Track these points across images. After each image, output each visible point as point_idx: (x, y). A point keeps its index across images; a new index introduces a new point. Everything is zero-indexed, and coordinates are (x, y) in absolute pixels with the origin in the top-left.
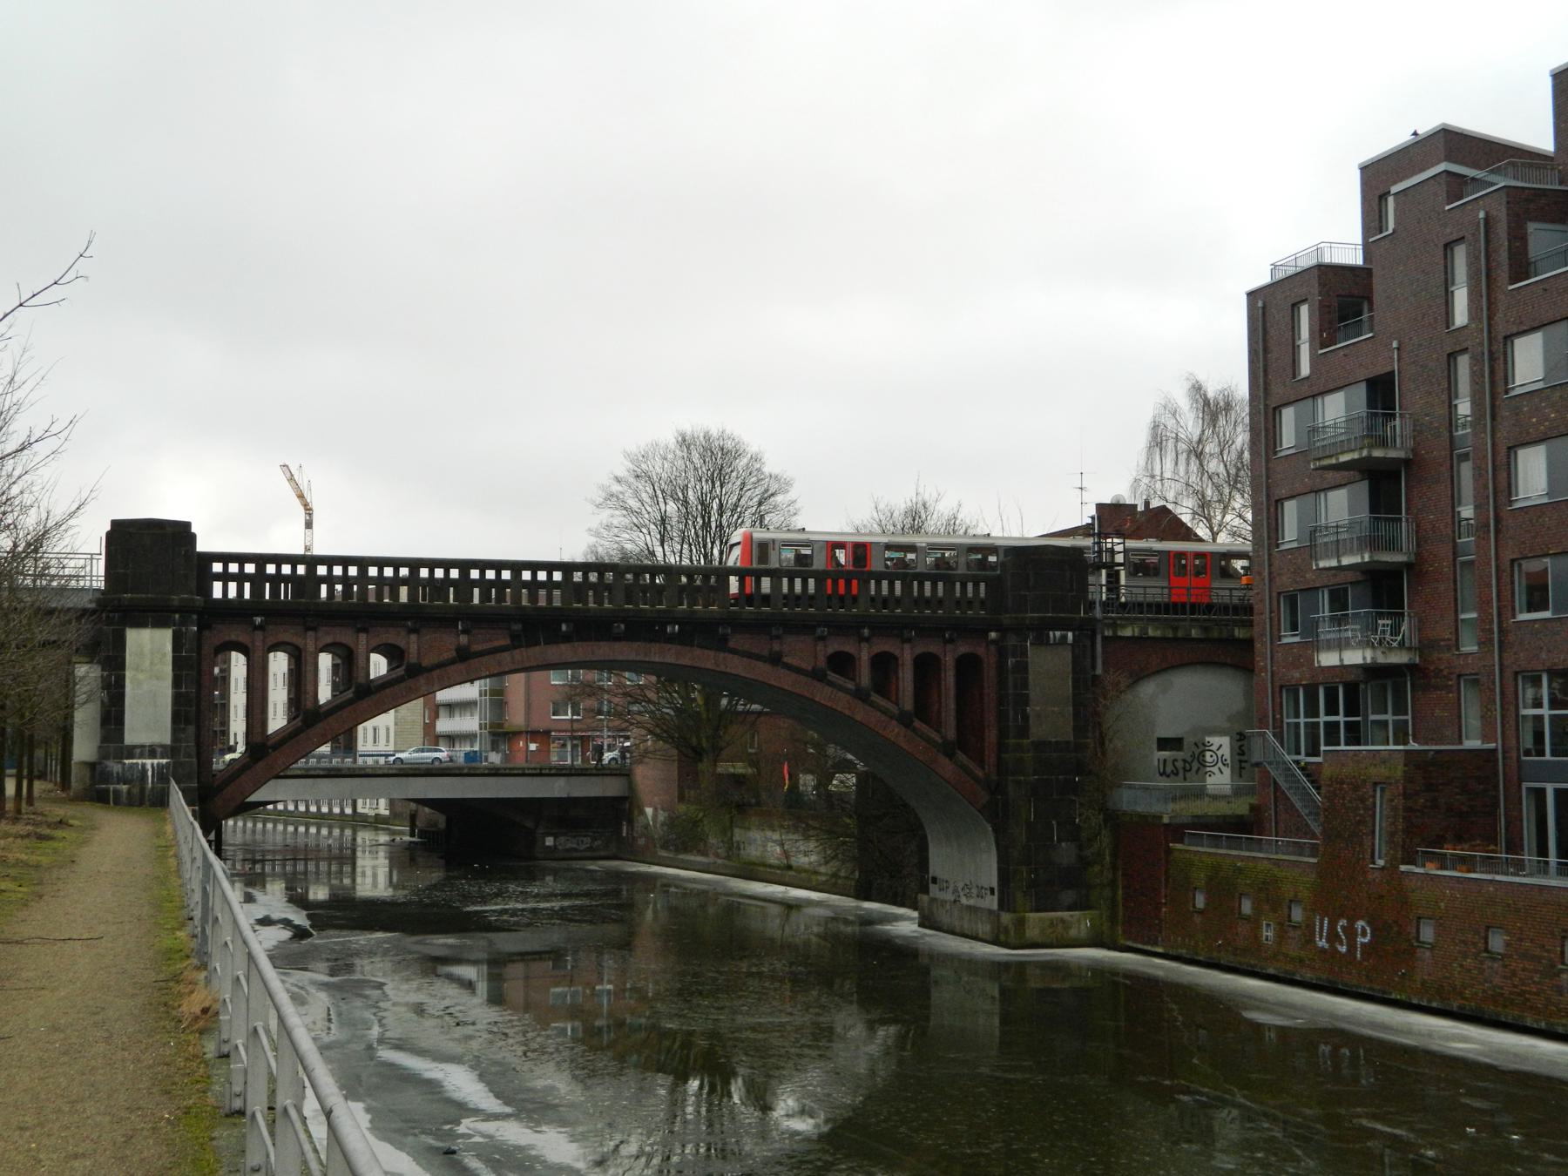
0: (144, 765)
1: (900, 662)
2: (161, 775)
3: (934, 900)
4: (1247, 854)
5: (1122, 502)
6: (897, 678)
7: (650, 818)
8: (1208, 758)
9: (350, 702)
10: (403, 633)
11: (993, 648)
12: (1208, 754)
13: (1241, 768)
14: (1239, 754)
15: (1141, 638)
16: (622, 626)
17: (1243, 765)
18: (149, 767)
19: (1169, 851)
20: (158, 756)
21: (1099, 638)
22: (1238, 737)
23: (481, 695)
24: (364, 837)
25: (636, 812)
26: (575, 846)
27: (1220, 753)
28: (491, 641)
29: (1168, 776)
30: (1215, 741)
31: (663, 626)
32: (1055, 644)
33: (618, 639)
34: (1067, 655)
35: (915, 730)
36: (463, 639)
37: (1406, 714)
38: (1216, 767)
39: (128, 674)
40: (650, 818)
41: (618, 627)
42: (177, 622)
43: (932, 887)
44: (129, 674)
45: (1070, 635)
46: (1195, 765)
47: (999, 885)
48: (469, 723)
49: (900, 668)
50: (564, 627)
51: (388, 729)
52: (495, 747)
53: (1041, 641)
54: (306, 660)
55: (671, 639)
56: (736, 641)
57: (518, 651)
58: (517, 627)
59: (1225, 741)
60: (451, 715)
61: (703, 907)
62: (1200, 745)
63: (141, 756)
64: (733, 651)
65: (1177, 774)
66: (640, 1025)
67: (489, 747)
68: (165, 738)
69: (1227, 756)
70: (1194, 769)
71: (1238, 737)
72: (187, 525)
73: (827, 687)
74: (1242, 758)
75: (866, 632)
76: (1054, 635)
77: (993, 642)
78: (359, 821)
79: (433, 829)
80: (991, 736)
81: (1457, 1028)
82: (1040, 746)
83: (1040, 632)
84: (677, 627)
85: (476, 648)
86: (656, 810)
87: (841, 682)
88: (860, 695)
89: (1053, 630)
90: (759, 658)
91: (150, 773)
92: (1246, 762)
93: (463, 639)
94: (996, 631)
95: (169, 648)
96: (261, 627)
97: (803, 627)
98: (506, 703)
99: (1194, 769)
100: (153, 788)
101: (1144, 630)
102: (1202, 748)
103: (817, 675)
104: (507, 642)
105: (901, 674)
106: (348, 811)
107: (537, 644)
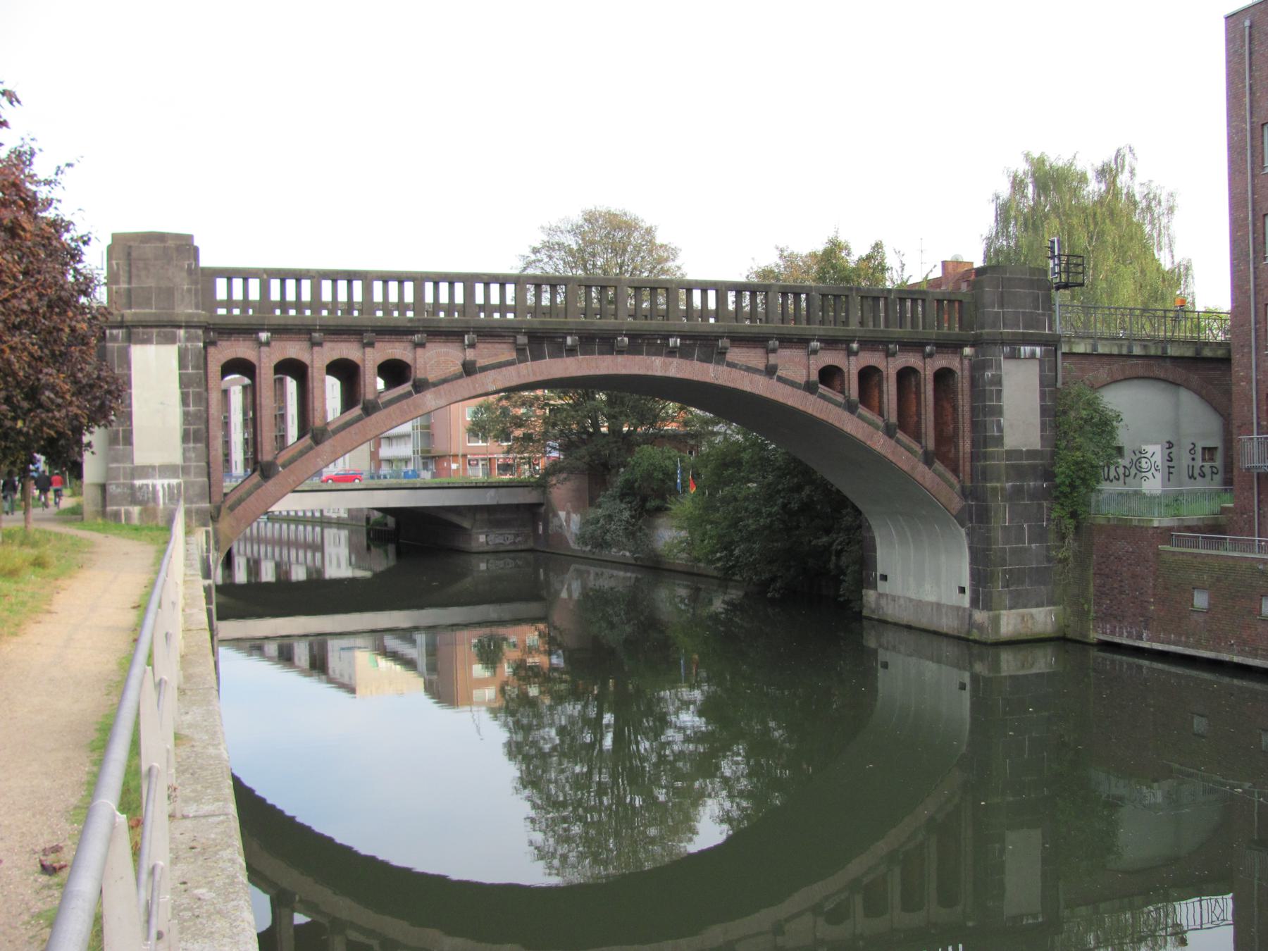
0: (154, 487)
1: (885, 376)
2: (172, 495)
3: (881, 595)
4: (1176, 549)
5: (960, 260)
6: (881, 392)
7: (563, 520)
8: (1144, 465)
9: (358, 419)
10: (409, 347)
11: (966, 362)
12: (1144, 461)
13: (1170, 473)
14: (1168, 461)
15: (1092, 354)
16: (626, 339)
17: (1172, 470)
19: (1158, 554)
21: (1059, 353)
22: (1167, 445)
23: (413, 429)
24: (330, 533)
25: (551, 515)
26: (502, 541)
27: (1153, 460)
28: (496, 355)
29: (1111, 481)
30: (1150, 449)
31: (666, 337)
32: (1025, 358)
33: (621, 352)
35: (898, 441)
36: (470, 354)
38: (1150, 472)
40: (563, 520)
41: (622, 340)
43: (880, 583)
46: (1133, 471)
47: (971, 585)
48: (405, 450)
49: (885, 382)
50: (569, 340)
52: (425, 467)
53: (1014, 356)
54: (313, 377)
55: (672, 352)
56: (735, 354)
57: (522, 365)
58: (522, 340)
59: (1157, 449)
60: (390, 444)
61: (313, 514)
62: (1137, 453)
64: (732, 365)
65: (1118, 479)
67: (421, 467)
68: (176, 458)
69: (1159, 463)
70: (1133, 474)
71: (1167, 445)
72: (190, 237)
73: (819, 400)
74: (1171, 464)
75: (855, 346)
79: (383, 528)
80: (965, 446)
82: (1011, 454)
84: (678, 340)
85: (481, 362)
86: (568, 513)
87: (831, 395)
88: (851, 407)
91: (161, 494)
92: (1173, 467)
93: (470, 354)
94: (972, 346)
96: (268, 344)
97: (800, 341)
98: (433, 435)
99: (1133, 474)
100: (165, 509)
101: (1095, 347)
102: (1139, 455)
103: (810, 388)
104: (514, 356)
105: (885, 388)
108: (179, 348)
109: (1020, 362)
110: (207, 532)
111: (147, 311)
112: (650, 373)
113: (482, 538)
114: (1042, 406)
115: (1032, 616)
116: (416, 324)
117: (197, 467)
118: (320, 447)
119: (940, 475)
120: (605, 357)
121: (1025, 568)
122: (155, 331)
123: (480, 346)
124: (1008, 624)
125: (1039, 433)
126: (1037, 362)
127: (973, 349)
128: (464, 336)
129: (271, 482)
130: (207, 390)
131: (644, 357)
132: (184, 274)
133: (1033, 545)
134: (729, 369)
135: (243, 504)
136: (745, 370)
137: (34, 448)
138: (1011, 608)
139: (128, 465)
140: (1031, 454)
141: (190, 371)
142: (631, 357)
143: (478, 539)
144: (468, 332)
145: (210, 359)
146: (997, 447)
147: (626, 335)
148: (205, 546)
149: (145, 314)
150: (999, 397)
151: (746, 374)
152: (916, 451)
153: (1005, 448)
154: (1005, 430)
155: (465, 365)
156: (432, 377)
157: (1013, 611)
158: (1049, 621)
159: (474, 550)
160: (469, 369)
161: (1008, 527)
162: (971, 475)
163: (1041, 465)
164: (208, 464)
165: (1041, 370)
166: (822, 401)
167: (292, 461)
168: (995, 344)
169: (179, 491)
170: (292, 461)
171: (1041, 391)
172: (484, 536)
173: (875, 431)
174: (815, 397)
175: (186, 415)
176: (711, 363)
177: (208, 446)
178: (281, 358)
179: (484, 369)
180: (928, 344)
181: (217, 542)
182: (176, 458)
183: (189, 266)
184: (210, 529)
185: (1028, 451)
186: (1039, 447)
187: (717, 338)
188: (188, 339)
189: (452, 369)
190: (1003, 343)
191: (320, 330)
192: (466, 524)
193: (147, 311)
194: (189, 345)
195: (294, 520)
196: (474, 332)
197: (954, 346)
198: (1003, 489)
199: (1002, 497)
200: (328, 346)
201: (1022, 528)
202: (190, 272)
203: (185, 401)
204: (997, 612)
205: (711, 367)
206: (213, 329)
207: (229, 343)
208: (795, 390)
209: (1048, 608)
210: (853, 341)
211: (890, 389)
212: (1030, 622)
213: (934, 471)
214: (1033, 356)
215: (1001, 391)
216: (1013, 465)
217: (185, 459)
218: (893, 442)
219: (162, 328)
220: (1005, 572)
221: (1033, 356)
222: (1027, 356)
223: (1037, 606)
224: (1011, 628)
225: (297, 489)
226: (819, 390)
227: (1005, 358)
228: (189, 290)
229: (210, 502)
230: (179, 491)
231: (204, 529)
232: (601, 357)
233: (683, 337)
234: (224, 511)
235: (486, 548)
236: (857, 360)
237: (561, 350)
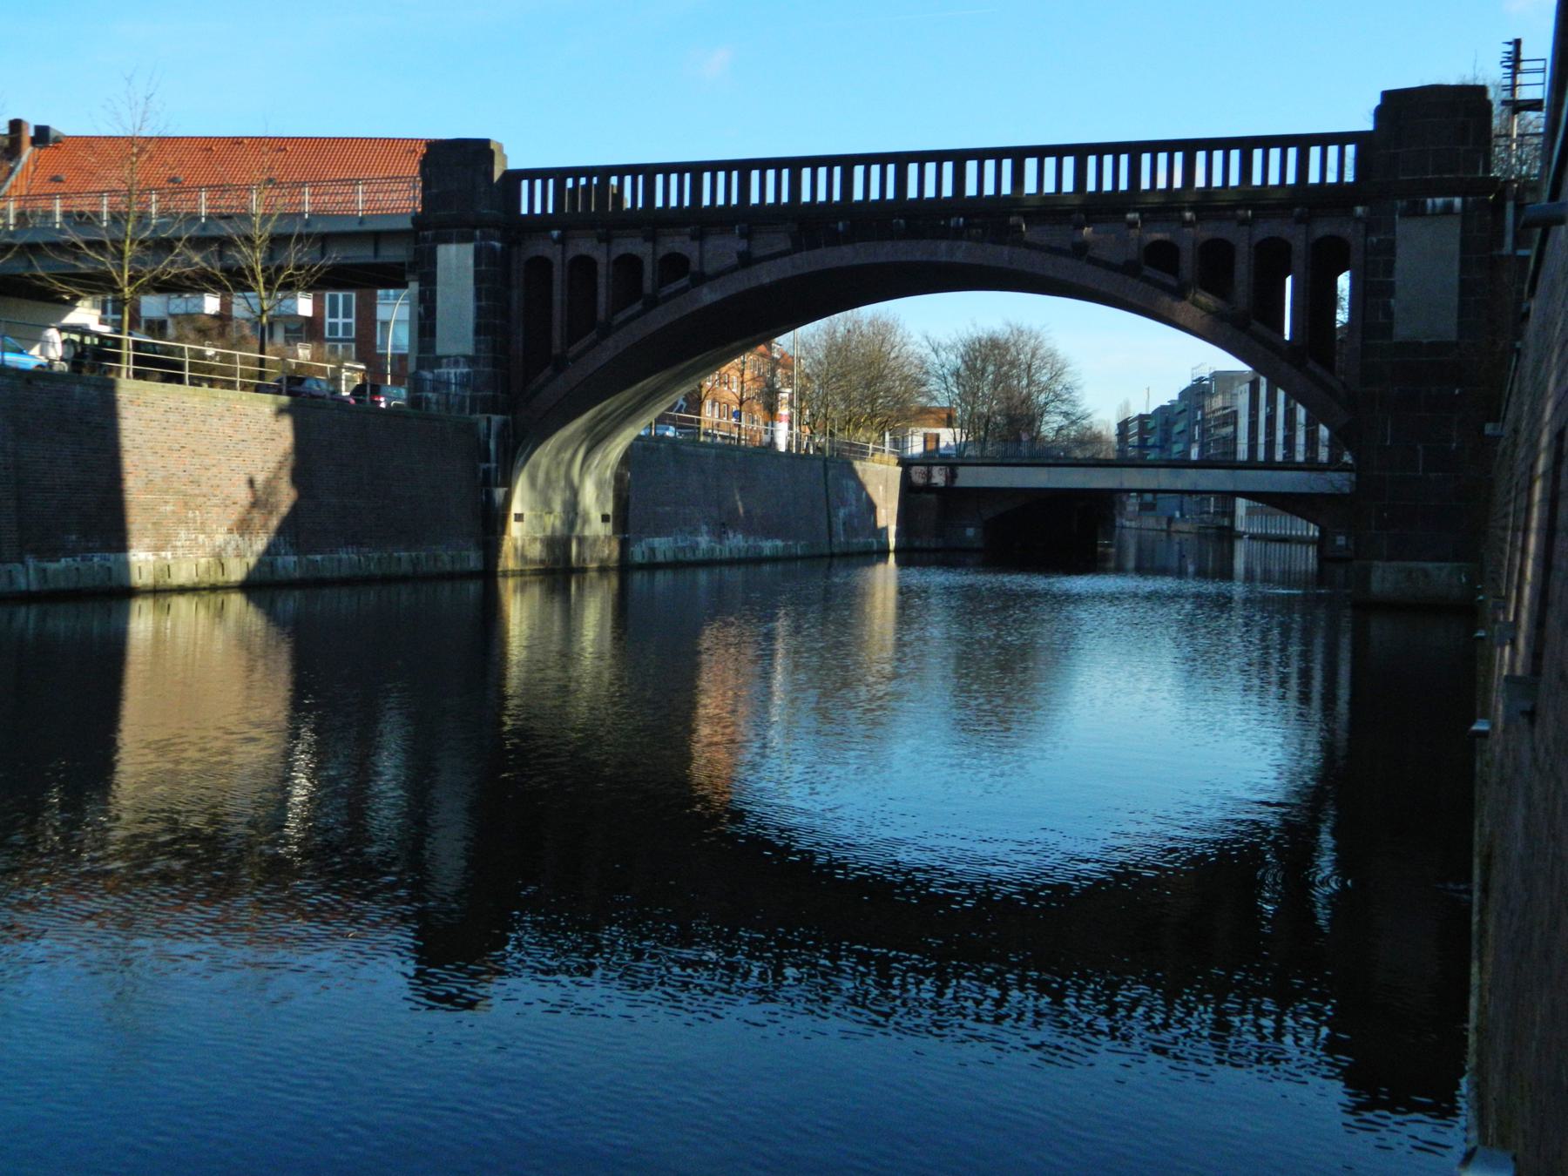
11: (1361, 227)
18: (452, 376)
20: (444, 365)
32: (1434, 214)
34: (1454, 228)
37: (235, 355)
39: (439, 288)
41: (898, 223)
42: (478, 237)
44: (439, 288)
45: (1457, 201)
53: (1416, 211)
57: (797, 255)
63: (448, 366)
66: (121, 290)
76: (1434, 204)
77: (1359, 219)
78: (1286, 529)
81: (609, 405)
84: (961, 220)
89: (1432, 196)
95: (471, 262)
107: (818, 246)
112: (934, 259)
114: (1462, 282)
115: (1426, 574)
127: (1367, 209)
128: (734, 226)
133: (1432, 475)
134: (1027, 251)
137: (1293, 628)
138: (1390, 559)
139: (432, 355)
141: (483, 268)
143: (1335, 541)
155: (740, 255)
157: (1394, 564)
160: (746, 260)
165: (1464, 230)
176: (1005, 244)
186: (1453, 337)
188: (482, 238)
203: (478, 296)
205: (1006, 250)
209: (1456, 564)
210: (1183, 209)
211: (1243, 269)
214: (1448, 209)
215: (1394, 262)
217: (477, 350)
221: (1448, 209)
222: (1438, 210)
227: (1400, 216)
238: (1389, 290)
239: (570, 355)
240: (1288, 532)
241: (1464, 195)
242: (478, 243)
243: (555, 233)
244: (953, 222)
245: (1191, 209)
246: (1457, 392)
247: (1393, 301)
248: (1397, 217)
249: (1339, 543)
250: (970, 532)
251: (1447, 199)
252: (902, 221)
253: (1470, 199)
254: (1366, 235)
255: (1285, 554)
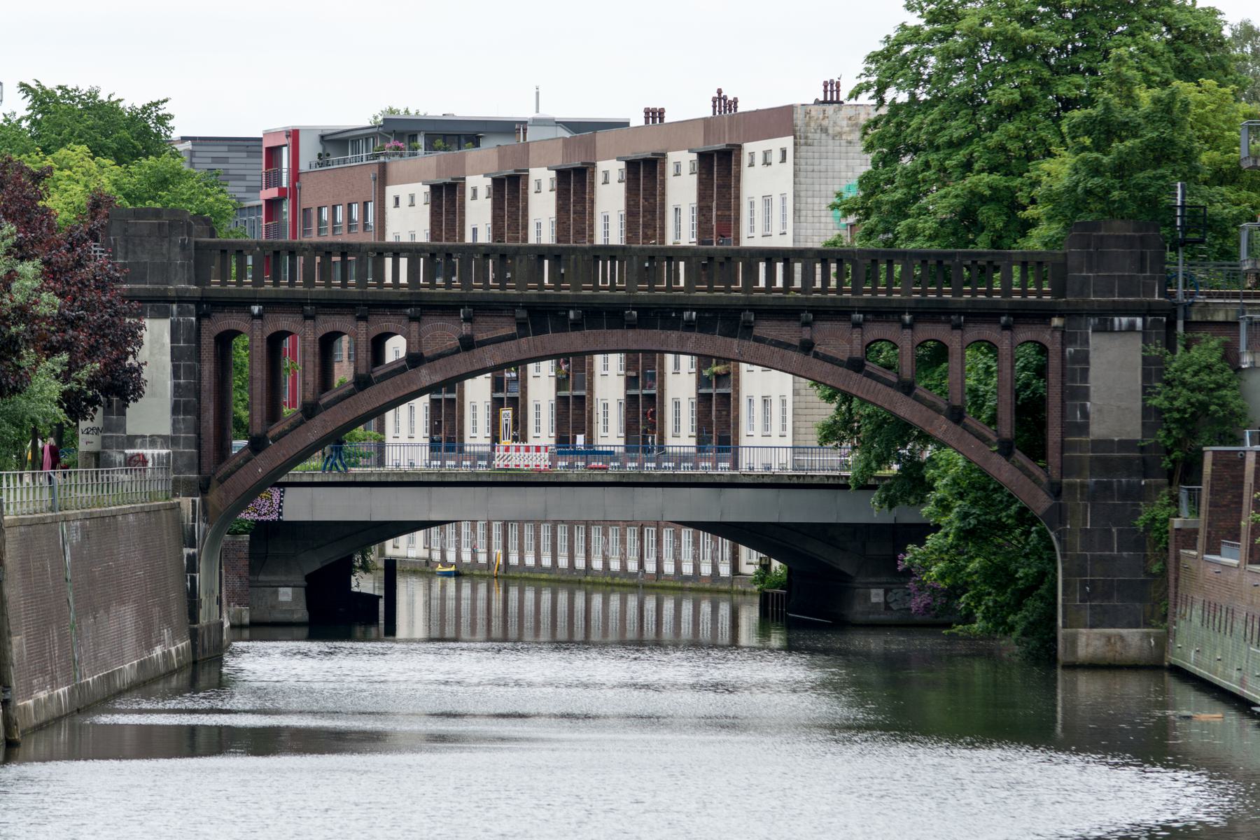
10: (405, 321)
11: (1058, 335)
16: (635, 313)
31: (681, 309)
33: (631, 326)
41: (630, 314)
45: (1139, 321)
50: (572, 314)
51: (784, 402)
53: (1105, 328)
56: (766, 329)
57: (523, 340)
58: (521, 314)
68: (166, 430)
73: (865, 378)
75: (907, 318)
76: (1120, 321)
77: (1056, 328)
80: (1054, 435)
82: (1098, 444)
83: (1104, 318)
84: (694, 314)
90: (787, 346)
93: (465, 329)
94: (1061, 316)
96: (260, 316)
106: (725, 570)
108: (172, 322)
109: (1115, 336)
110: (194, 502)
111: (142, 286)
113: (877, 596)
115: (1122, 638)
116: (408, 298)
117: (185, 438)
118: (310, 422)
119: (1022, 469)
120: (615, 331)
121: (1113, 581)
122: (149, 305)
123: (479, 319)
124: (1087, 645)
125: (1140, 421)
126: (1139, 338)
129: (261, 456)
130: (199, 361)
131: (658, 331)
132: (177, 250)
133: (1125, 554)
134: (756, 344)
135: (233, 477)
136: (774, 346)
138: (1092, 627)
140: (1125, 445)
142: (643, 331)
143: (868, 597)
144: (463, 307)
145: (203, 330)
146: (1080, 435)
147: (634, 309)
148: (191, 516)
149: (139, 289)
150: (1085, 377)
151: (777, 349)
152: (989, 440)
153: (1091, 437)
154: (1091, 416)
156: (427, 352)
157: (1095, 630)
158: (1145, 644)
159: (860, 618)
161: (1089, 531)
162: (1062, 468)
163: (1138, 458)
164: (199, 435)
166: (870, 380)
167: (283, 434)
168: (1081, 315)
169: (168, 462)
170: (283, 434)
171: (1143, 369)
172: (881, 592)
173: (936, 415)
174: (860, 376)
175: (176, 387)
176: (735, 337)
177: (199, 418)
178: (274, 330)
179: (483, 343)
180: (1003, 315)
181: (205, 512)
182: (166, 430)
183: (183, 241)
184: (198, 499)
185: (1120, 441)
187: (739, 310)
188: (180, 314)
189: (448, 343)
190: (1091, 314)
191: (312, 304)
192: (846, 566)
193: (142, 286)
194: (181, 319)
195: (636, 586)
196: (469, 306)
197: (1040, 315)
198: (1083, 485)
199: (1082, 494)
200: (321, 318)
201: (1110, 531)
202: (183, 247)
203: (176, 373)
204: (1073, 630)
206: (207, 303)
207: (222, 315)
208: (836, 367)
210: (904, 313)
212: (1119, 644)
213: (1013, 463)
214: (1131, 328)
215: (1087, 370)
216: (1097, 458)
218: (959, 429)
219: (158, 304)
220: (1084, 584)
222: (1123, 329)
223: (1130, 626)
224: (1091, 650)
225: (283, 479)
226: (866, 368)
228: (182, 265)
229: (200, 473)
230: (168, 462)
231: (190, 499)
232: (609, 331)
233: (698, 310)
234: (214, 482)
235: (884, 617)
236: (862, 335)
237: (563, 325)
238: (1085, 393)
239: (271, 434)
240: (615, 565)
241: (1143, 316)
242: (175, 318)
243: (256, 309)
244: (686, 315)
245: (910, 313)
246: (1143, 483)
247: (1088, 404)
248: (1090, 331)
249: (874, 600)
250: (286, 594)
251: (1131, 318)
252: (635, 313)
253: (1149, 319)
254: (1064, 346)
255: (443, 599)
